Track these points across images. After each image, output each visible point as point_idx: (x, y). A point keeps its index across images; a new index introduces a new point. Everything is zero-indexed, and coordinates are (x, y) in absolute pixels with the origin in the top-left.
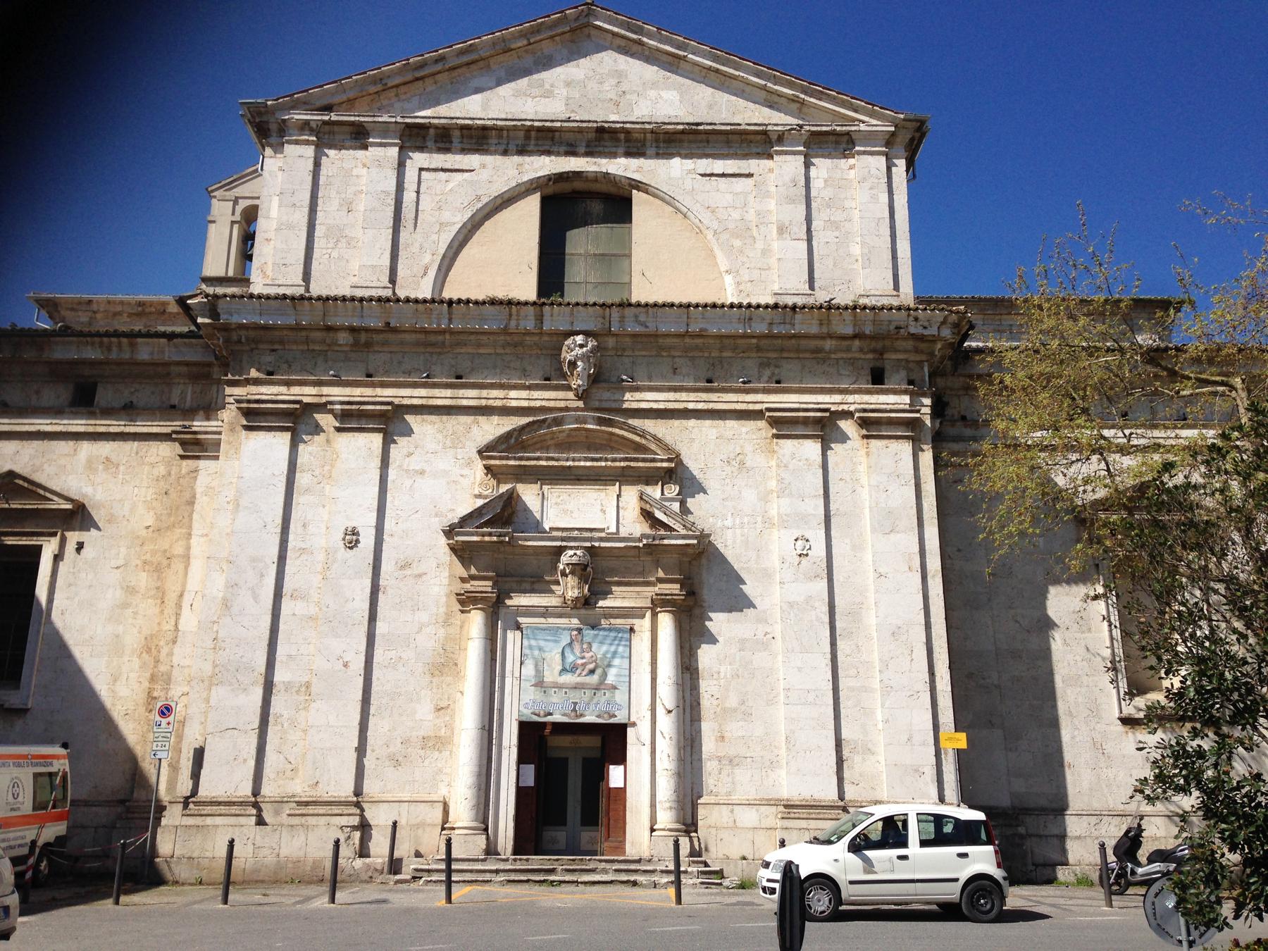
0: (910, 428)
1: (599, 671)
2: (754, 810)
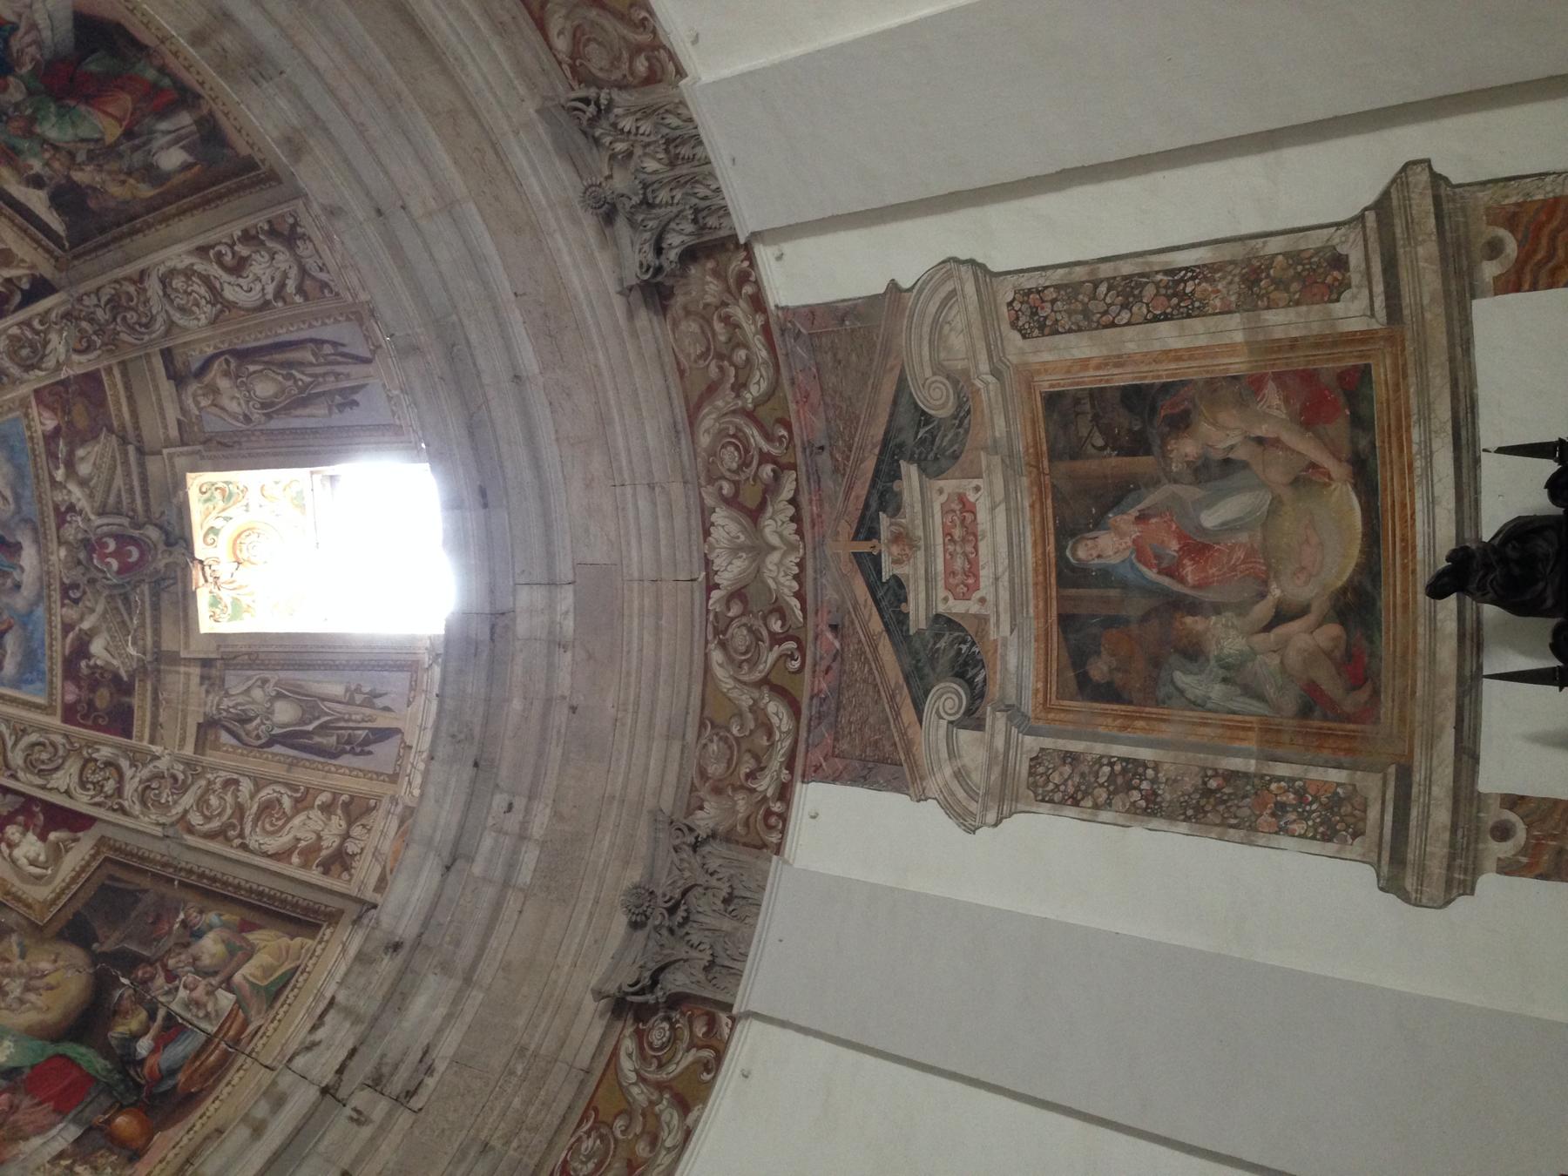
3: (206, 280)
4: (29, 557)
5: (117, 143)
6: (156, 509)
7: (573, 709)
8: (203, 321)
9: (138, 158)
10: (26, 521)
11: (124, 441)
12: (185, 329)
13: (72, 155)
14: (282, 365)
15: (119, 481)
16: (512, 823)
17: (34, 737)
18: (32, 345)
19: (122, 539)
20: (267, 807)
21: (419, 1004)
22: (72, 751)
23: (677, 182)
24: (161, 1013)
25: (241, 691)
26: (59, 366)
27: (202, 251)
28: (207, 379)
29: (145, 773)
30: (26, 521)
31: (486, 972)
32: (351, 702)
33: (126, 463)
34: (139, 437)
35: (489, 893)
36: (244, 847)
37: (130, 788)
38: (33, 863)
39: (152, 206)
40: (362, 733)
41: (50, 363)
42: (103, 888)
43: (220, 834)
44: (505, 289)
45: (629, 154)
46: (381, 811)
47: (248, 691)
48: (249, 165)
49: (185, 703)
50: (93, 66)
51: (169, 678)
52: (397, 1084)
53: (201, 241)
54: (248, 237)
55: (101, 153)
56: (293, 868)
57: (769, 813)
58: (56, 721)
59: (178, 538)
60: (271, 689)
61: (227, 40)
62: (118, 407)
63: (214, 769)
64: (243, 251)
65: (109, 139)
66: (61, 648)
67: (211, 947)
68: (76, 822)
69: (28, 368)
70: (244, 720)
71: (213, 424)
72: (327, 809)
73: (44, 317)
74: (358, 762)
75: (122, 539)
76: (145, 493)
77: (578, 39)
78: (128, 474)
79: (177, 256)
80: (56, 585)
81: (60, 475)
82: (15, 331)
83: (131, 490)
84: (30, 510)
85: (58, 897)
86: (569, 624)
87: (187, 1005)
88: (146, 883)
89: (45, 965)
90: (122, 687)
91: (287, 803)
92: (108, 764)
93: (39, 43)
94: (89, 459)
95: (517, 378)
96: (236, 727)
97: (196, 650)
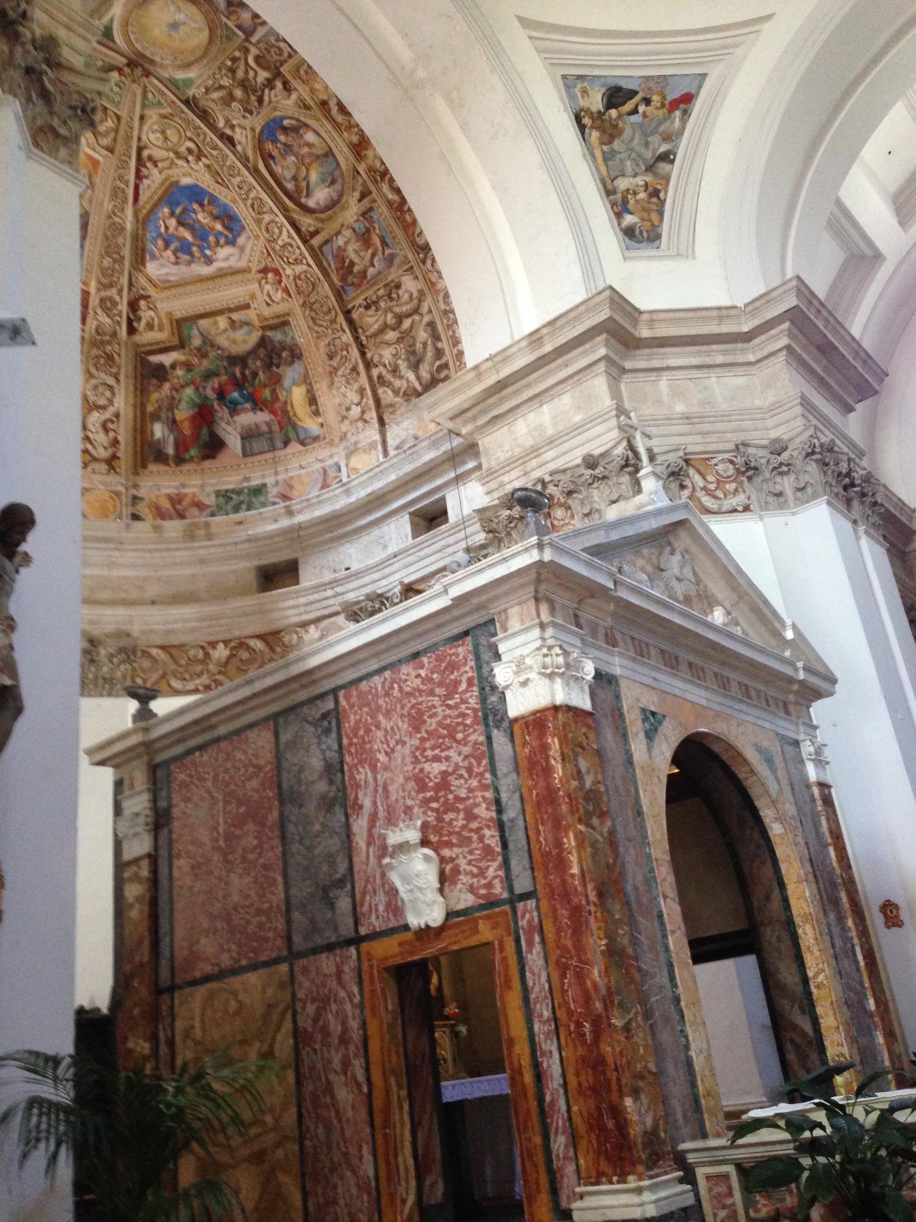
3: (104, 408)
5: (173, 414)
13: (177, 390)
23: (96, 678)
39: (143, 406)
41: (99, 311)
45: (111, 662)
48: (144, 466)
50: (205, 431)
54: (115, 442)
55: (173, 404)
61: (202, 532)
64: (112, 434)
65: (176, 412)
73: (119, 323)
77: (154, 660)
82: (119, 307)
93: (222, 418)
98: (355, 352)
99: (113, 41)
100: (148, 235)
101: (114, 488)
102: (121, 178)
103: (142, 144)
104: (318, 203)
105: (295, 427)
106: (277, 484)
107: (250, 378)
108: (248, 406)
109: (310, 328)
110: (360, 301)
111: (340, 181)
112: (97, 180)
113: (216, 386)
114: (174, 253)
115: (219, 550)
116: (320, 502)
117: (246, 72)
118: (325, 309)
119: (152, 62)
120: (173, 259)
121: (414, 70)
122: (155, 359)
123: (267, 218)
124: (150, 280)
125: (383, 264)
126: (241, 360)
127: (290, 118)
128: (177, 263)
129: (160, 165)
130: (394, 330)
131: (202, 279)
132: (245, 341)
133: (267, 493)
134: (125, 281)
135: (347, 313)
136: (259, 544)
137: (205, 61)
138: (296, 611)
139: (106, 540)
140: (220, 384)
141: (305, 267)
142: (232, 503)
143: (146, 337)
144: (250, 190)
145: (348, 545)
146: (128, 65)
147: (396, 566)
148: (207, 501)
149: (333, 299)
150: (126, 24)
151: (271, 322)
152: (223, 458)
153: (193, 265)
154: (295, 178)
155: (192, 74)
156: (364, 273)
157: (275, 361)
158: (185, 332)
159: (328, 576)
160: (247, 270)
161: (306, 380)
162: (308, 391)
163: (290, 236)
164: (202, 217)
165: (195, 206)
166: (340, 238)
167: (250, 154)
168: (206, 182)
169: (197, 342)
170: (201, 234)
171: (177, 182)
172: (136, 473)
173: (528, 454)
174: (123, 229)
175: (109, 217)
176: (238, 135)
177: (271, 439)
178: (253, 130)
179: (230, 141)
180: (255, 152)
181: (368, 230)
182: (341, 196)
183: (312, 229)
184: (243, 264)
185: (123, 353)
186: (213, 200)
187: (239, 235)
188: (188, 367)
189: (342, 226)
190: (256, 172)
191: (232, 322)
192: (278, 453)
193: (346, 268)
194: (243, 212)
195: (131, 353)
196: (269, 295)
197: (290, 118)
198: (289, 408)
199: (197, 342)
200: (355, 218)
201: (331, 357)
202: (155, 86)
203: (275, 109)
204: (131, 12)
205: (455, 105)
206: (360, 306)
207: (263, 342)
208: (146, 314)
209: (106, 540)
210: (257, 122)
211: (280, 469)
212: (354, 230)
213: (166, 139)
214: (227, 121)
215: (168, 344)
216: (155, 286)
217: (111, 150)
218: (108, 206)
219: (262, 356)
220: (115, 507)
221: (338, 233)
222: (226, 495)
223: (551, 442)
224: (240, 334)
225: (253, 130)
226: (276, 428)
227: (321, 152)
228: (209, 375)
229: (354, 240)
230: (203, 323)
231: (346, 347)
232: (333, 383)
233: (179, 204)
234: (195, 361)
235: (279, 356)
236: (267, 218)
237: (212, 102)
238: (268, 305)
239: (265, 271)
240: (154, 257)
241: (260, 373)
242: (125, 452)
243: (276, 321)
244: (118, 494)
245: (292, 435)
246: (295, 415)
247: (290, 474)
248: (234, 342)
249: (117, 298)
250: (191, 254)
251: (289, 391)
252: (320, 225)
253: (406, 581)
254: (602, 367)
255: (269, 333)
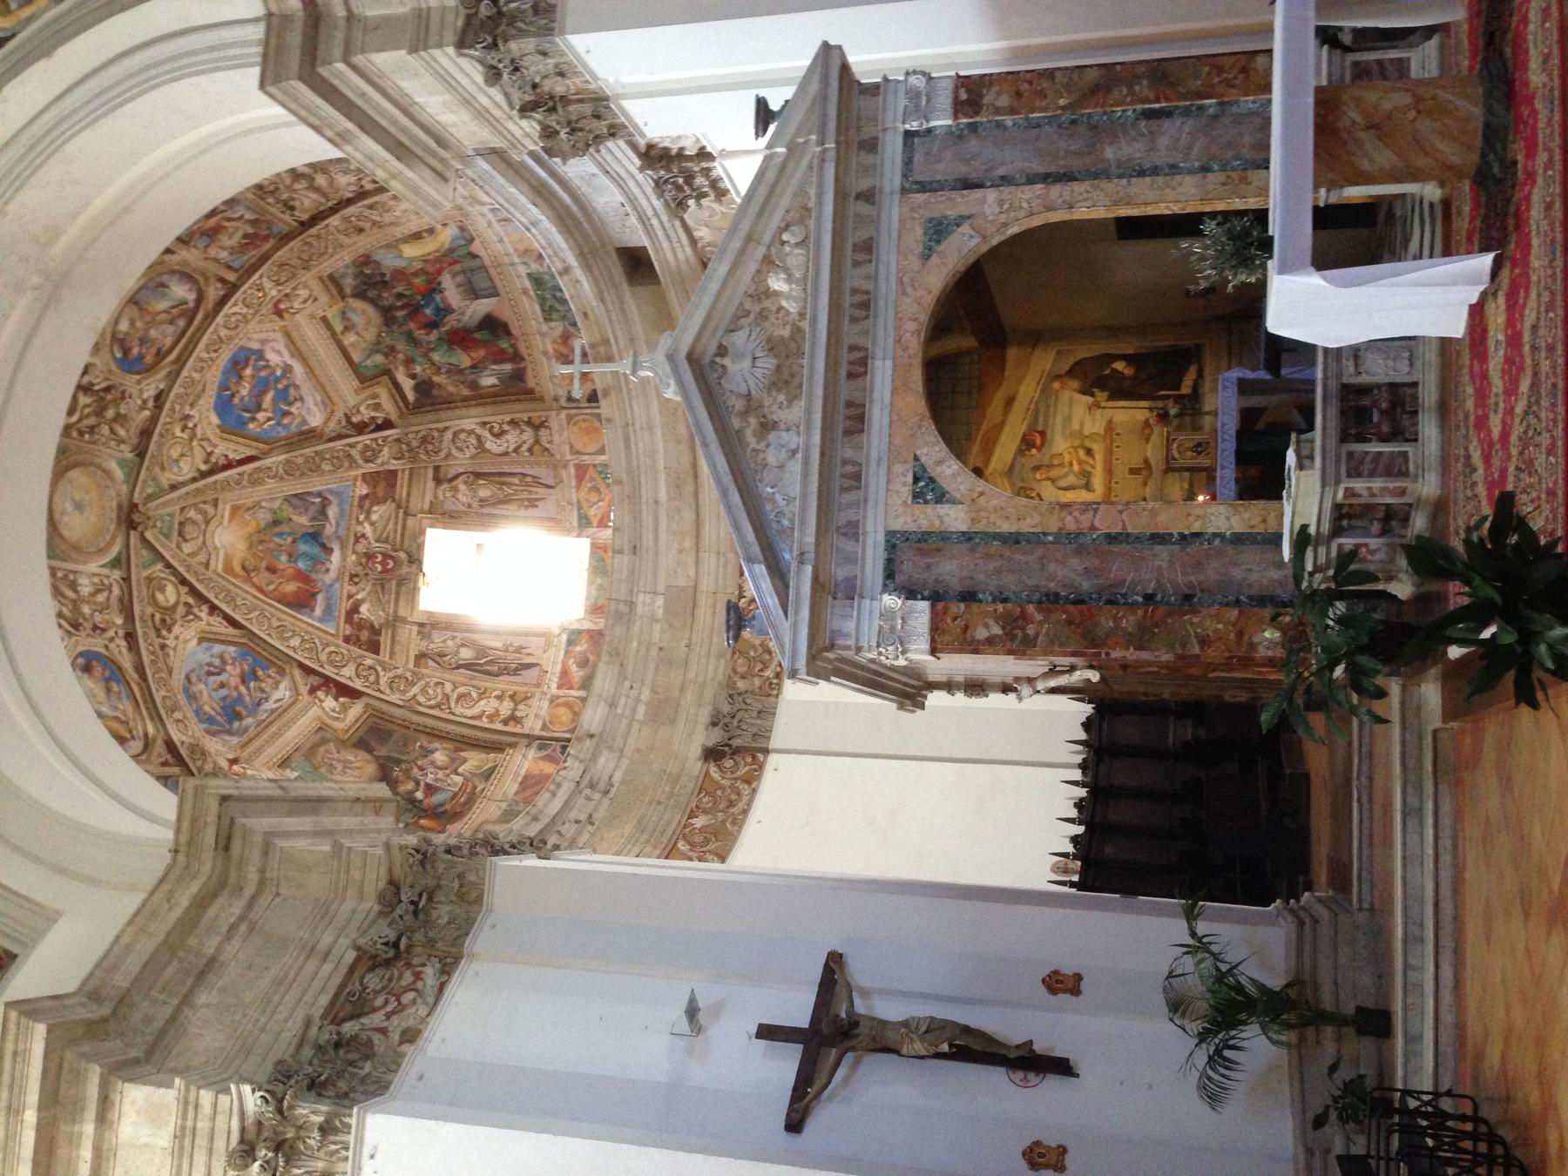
0: (1288, 1045)
1: (1088, 444)
2: (166, 1145)
3: (479, 438)
4: (336, 557)
6: (406, 544)
7: (661, 649)
8: (468, 455)
9: (470, 378)
10: (339, 538)
11: (399, 507)
12: (456, 458)
13: (439, 369)
14: (498, 483)
15: (391, 526)
16: (633, 693)
17: (332, 649)
18: (373, 450)
19: (386, 556)
20: (461, 697)
21: (602, 760)
22: (351, 658)
24: (422, 783)
25: (438, 641)
26: (383, 464)
27: (484, 424)
28: (454, 483)
29: (390, 674)
30: (339, 538)
31: (628, 751)
32: (507, 651)
33: (397, 517)
34: (407, 507)
35: (625, 722)
36: (453, 714)
37: (383, 680)
38: (333, 711)
39: (465, 399)
40: (514, 666)
41: (379, 461)
42: (371, 728)
43: (438, 706)
44: (661, 464)
46: (536, 699)
47: (444, 641)
48: (532, 392)
49: (409, 643)
50: (478, 336)
51: (400, 631)
52: (602, 786)
53: (485, 419)
55: (454, 371)
56: (484, 723)
57: (771, 684)
58: (340, 642)
59: (415, 560)
60: (458, 641)
62: (402, 490)
63: (428, 676)
64: (506, 427)
65: (463, 366)
66: (346, 606)
67: (440, 757)
68: (353, 694)
69: (367, 461)
70: (442, 655)
71: (450, 505)
72: (498, 698)
73: (385, 439)
74: (513, 678)
75: (386, 556)
76: (403, 535)
78: (396, 523)
79: (469, 424)
80: (347, 574)
81: (362, 517)
82: (368, 442)
83: (396, 532)
84: (342, 533)
85: (350, 728)
86: (660, 612)
87: (436, 780)
88: (396, 728)
89: (351, 758)
90: (375, 631)
91: (474, 695)
92: (370, 668)
94: (378, 512)
95: (656, 502)
96: (437, 658)
97: (416, 618)
98: (351, 210)
99: (120, 553)
100: (284, 434)
101: (564, 422)
102: (238, 483)
103: (197, 475)
104: (190, 290)
105: (451, 250)
106: (526, 264)
107: (405, 300)
108: (438, 298)
109: (332, 256)
110: (287, 217)
111: (158, 279)
112: (249, 502)
113: (422, 332)
114: (290, 404)
115: (617, 326)
116: (550, 245)
117: (88, 416)
118: (306, 248)
119: (120, 506)
120: (298, 404)
121: (36, 288)
122: (411, 396)
123: (223, 332)
124: (329, 419)
125: (238, 208)
126: (387, 314)
127: (112, 353)
128: (302, 399)
129: (209, 450)
130: (313, 179)
131: (310, 370)
132: (364, 312)
133: (539, 273)
134: (338, 444)
135: (305, 225)
136: (604, 288)
137: (97, 460)
138: (679, 249)
139: (627, 439)
140: (420, 329)
141: (264, 279)
142: (557, 305)
143: (389, 408)
144: (202, 360)
145: (595, 204)
146: (135, 529)
147: (618, 169)
148: (560, 330)
149: (292, 244)
150: (101, 552)
151: (335, 292)
152: (505, 315)
153: (297, 383)
154: (171, 322)
155: (113, 466)
156: (253, 223)
157: (379, 279)
158: (371, 373)
159: (633, 220)
160: (287, 334)
161: (393, 246)
162: (406, 242)
163: (235, 304)
164: (245, 389)
165: (236, 401)
166: (220, 257)
167: (164, 372)
168: (208, 401)
169: (379, 359)
170: (261, 388)
171: (219, 427)
172: (541, 399)
173: (487, 120)
174: (288, 461)
175: (282, 479)
176: (150, 392)
177: (472, 270)
178: (139, 382)
179: (160, 398)
180: (159, 371)
181: (203, 234)
182: (173, 272)
183: (219, 285)
184: (278, 336)
185: (416, 428)
186: (224, 387)
187: (250, 349)
188: (409, 362)
189: (206, 259)
190: (181, 361)
191: (346, 329)
192: (487, 263)
193: (251, 240)
194: (225, 355)
195: (413, 419)
196: (305, 301)
197: (112, 353)
198: (431, 257)
199: (379, 359)
200: (193, 250)
201: (361, 230)
202: (140, 493)
203: (110, 371)
204: (89, 553)
205: (55, 233)
206: (292, 215)
207: (360, 295)
208: (366, 414)
209: (627, 439)
210: (129, 382)
211: (506, 260)
212: (207, 247)
213: (182, 455)
214: (142, 409)
215: (391, 386)
216: (333, 411)
217: (215, 503)
218: (271, 484)
219: (375, 292)
220: (584, 421)
221: (216, 260)
222: (548, 313)
223: (468, 102)
224: (358, 319)
225: (139, 382)
226: (458, 267)
227: (135, 309)
228: (412, 340)
229: (219, 244)
230: (356, 357)
231: (346, 219)
232: (392, 224)
233: (240, 416)
234: (400, 356)
235: (370, 276)
236: (223, 332)
237: (127, 432)
238: (316, 299)
239: (279, 313)
240: (304, 422)
241: (396, 290)
242: (521, 412)
243: (331, 287)
244: (570, 418)
245: (461, 252)
246: (436, 251)
247: (511, 251)
248: (368, 323)
249: (360, 447)
250: (287, 387)
251: (411, 259)
252: (212, 280)
253: (638, 163)
254: (359, 59)
255: (348, 291)
